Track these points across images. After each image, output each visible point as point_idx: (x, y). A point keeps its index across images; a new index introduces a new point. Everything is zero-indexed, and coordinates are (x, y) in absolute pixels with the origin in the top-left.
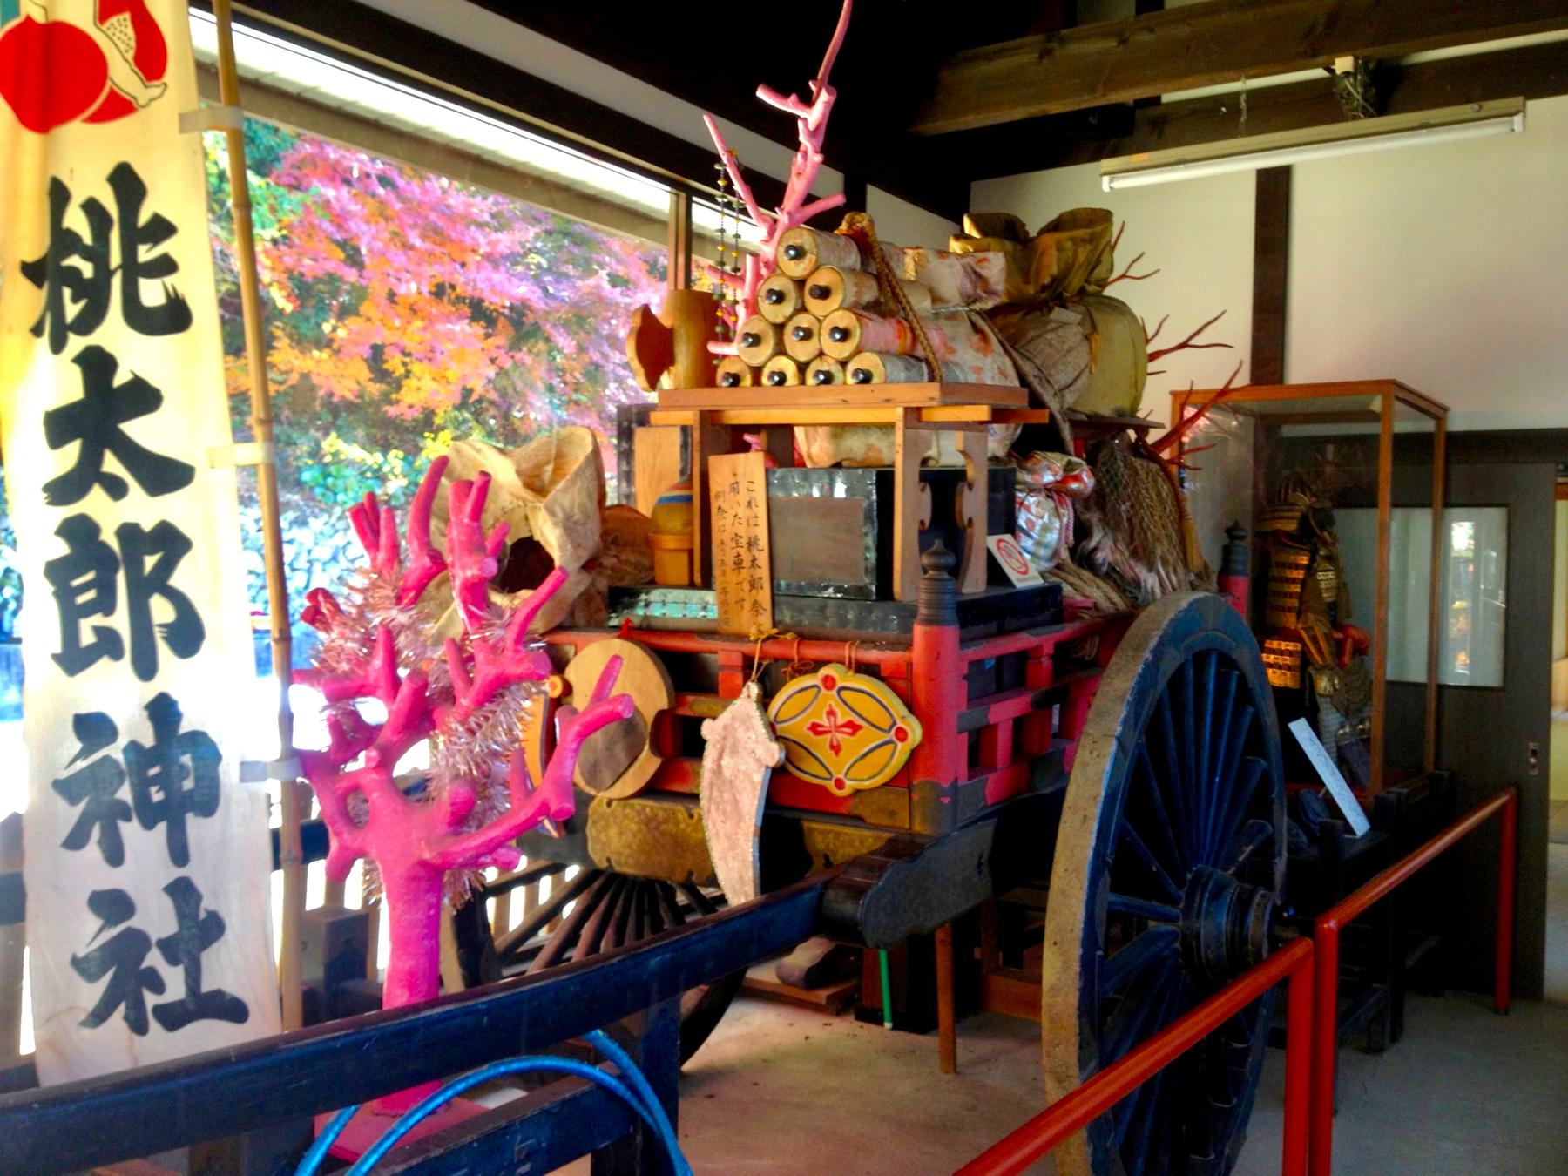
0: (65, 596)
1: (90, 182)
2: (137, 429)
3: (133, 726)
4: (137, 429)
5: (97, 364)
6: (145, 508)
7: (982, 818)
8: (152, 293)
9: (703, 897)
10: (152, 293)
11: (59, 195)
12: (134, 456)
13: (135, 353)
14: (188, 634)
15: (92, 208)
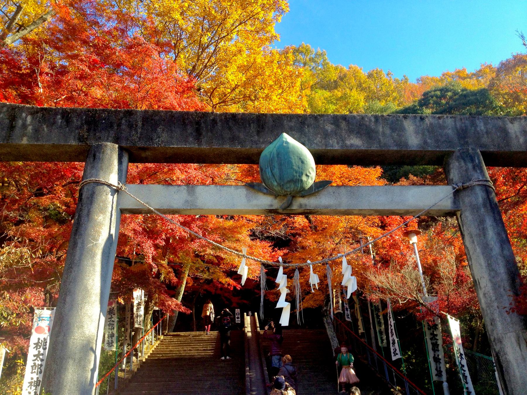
0: (32, 368)
5: (39, 352)
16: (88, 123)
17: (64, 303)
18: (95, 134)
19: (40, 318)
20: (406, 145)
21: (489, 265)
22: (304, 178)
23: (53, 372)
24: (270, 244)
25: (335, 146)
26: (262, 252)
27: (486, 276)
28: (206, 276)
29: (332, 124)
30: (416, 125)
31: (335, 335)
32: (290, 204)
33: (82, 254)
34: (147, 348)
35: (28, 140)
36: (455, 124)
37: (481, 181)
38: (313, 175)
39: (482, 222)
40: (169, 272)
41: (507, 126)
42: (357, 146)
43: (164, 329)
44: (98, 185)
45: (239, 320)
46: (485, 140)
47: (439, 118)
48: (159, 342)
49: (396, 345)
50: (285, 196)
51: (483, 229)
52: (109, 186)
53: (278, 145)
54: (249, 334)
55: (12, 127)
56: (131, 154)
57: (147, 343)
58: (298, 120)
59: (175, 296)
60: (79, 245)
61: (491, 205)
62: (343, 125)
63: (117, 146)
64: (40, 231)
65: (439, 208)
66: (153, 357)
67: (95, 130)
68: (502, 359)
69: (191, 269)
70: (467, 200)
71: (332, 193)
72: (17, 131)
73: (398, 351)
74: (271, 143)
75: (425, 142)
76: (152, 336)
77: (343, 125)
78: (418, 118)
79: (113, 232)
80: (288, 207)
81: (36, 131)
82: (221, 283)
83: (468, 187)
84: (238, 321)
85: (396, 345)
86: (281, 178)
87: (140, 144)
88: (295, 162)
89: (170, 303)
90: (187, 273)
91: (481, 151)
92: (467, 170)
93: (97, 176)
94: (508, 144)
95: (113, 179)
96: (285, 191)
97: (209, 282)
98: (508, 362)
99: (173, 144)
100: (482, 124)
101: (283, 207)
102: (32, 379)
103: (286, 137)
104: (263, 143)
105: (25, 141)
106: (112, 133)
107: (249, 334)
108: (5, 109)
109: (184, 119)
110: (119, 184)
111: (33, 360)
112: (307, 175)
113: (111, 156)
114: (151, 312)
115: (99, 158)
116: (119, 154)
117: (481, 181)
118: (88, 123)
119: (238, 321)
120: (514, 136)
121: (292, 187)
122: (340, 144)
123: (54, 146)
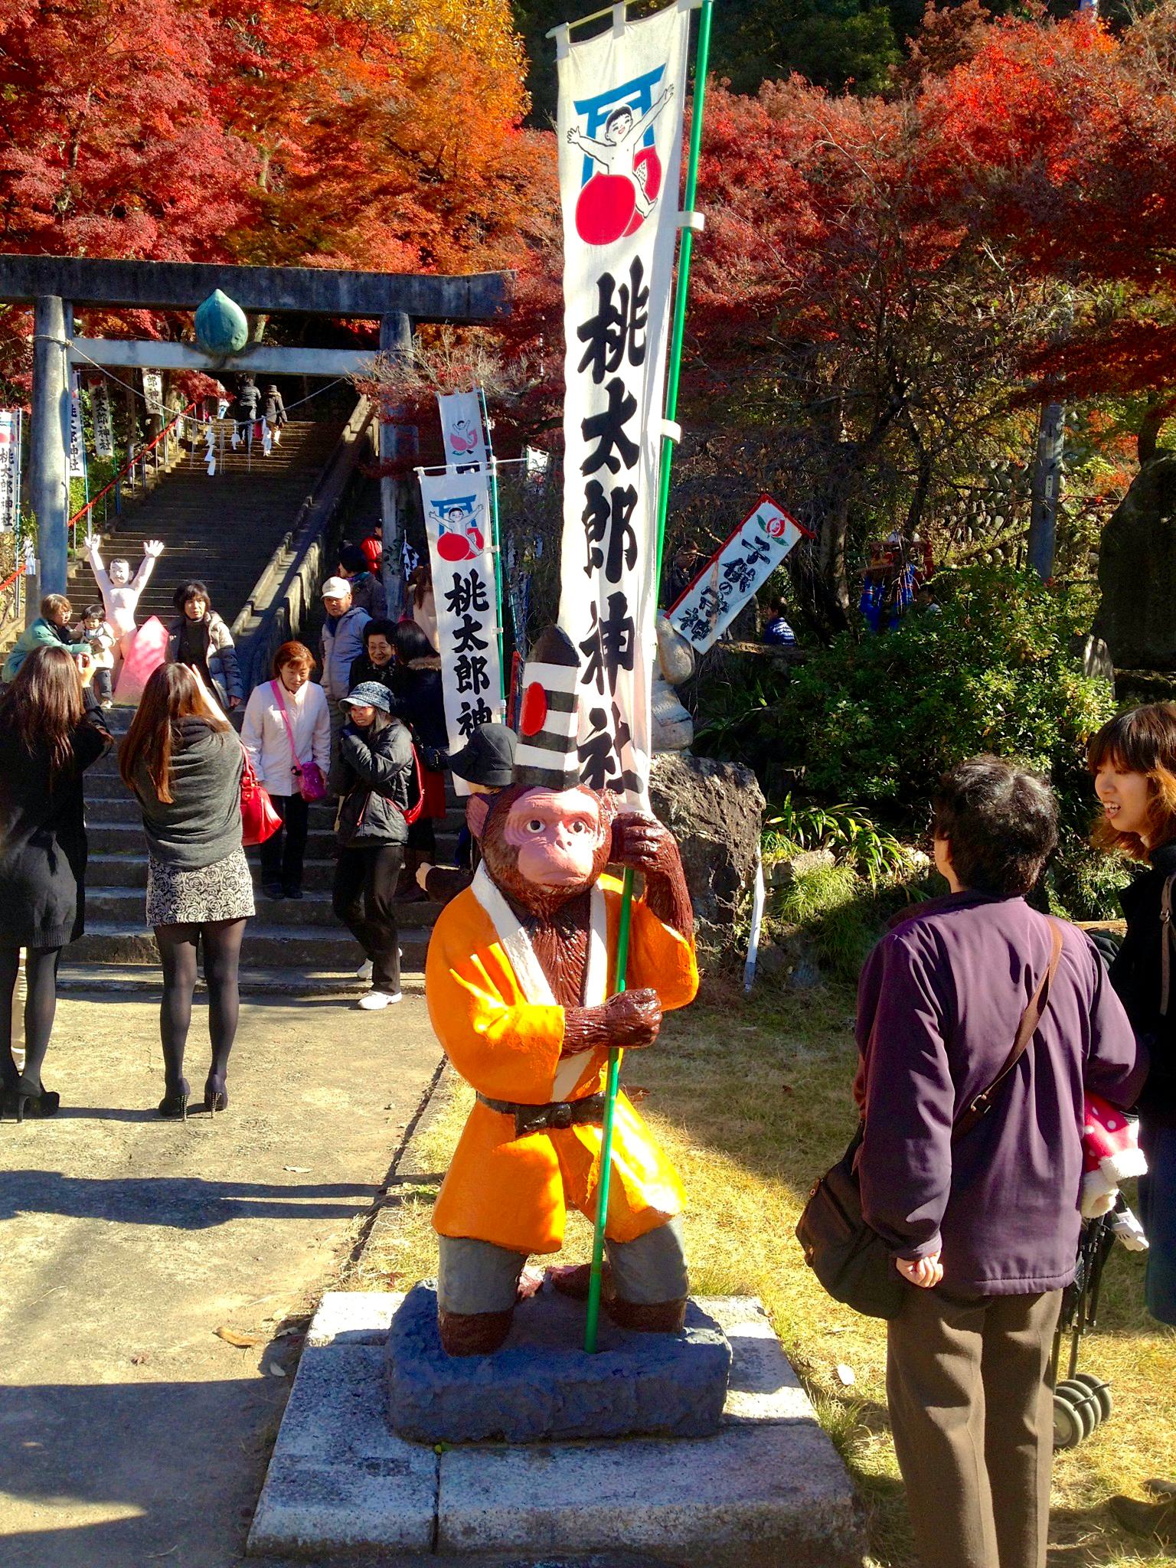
0: (459, 675)
1: (465, 575)
2: (477, 634)
3: (475, 706)
4: (477, 634)
5: (467, 618)
6: (478, 653)
7: (851, 1257)
8: (480, 601)
10: (480, 601)
11: (457, 577)
12: (475, 640)
14: (486, 683)
15: (466, 581)
22: (234, 341)
46: (416, 303)
56: (75, 307)
62: (278, 280)
75: (357, 304)
77: (278, 280)
88: (226, 325)
95: (60, 334)
102: (465, 706)
103: (220, 296)
106: (55, 285)
111: (457, 650)
120: (446, 300)
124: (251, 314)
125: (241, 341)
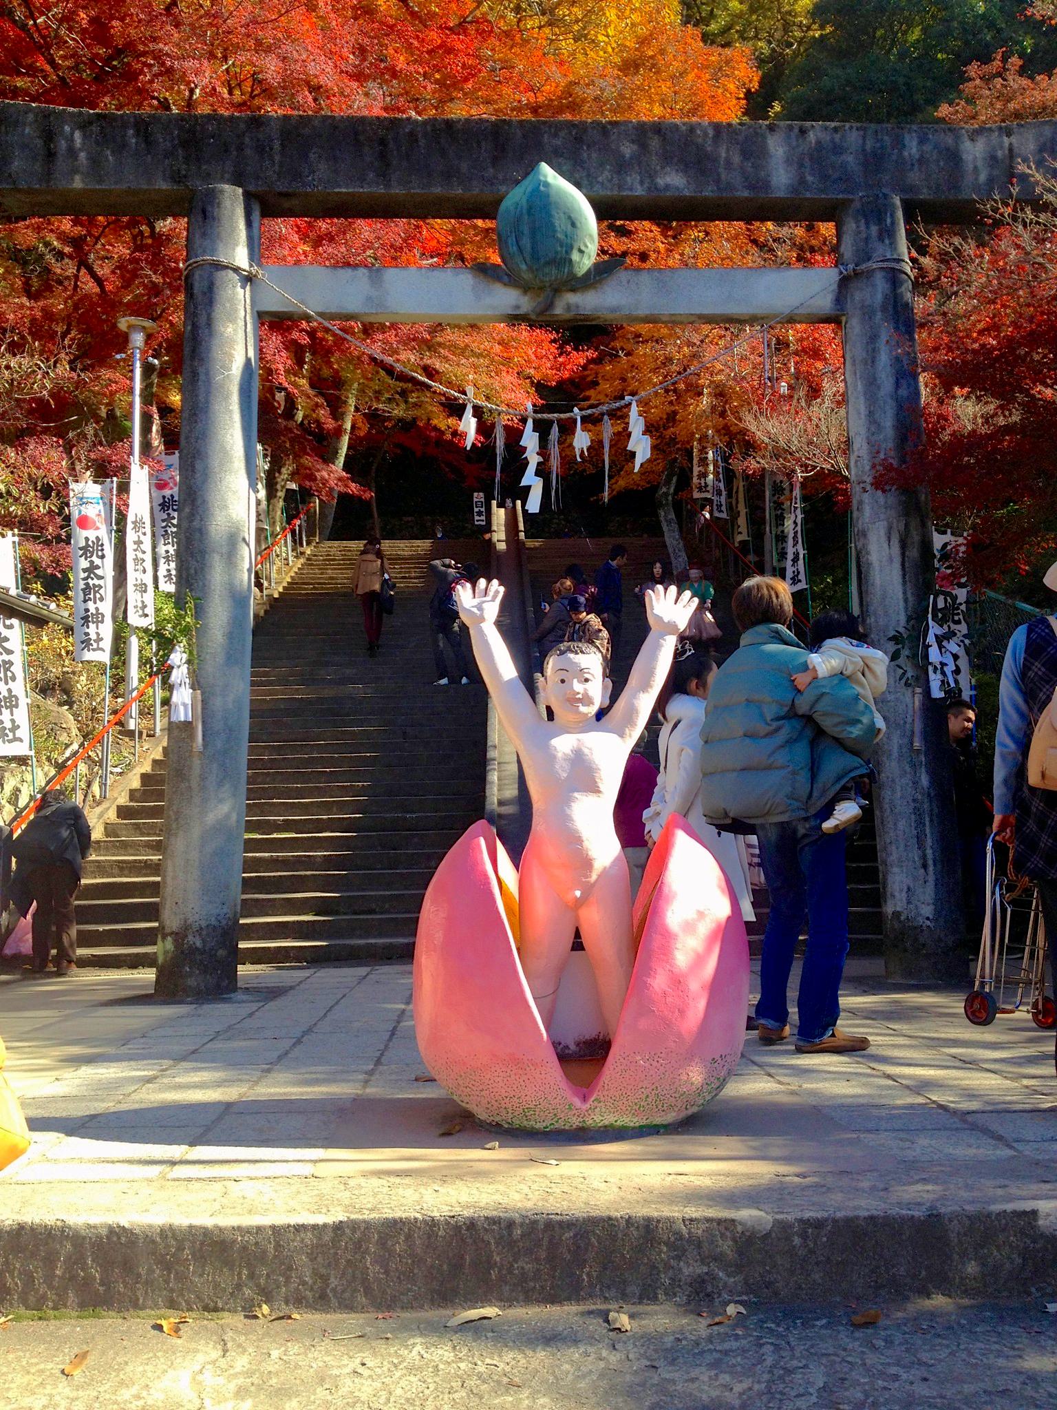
5: (91, 562)
6: (96, 582)
9: (597, 266)
13: (97, 561)
14: (14, 679)
16: (185, 144)
17: (193, 471)
18: (200, 168)
19: (83, 501)
20: (766, 185)
21: (871, 414)
22: (575, 256)
23: (192, 571)
24: (554, 336)
25: (636, 188)
26: (533, 357)
27: (863, 431)
28: (398, 412)
29: (633, 142)
30: (789, 145)
31: (681, 545)
32: (551, 305)
33: (208, 393)
34: (279, 571)
35: (83, 182)
36: (864, 143)
37: (888, 260)
38: (592, 248)
39: (873, 338)
40: (317, 405)
41: (962, 147)
42: (677, 189)
43: (311, 534)
44: (217, 270)
45: (483, 518)
46: (914, 177)
47: (836, 130)
48: (302, 560)
49: (801, 562)
50: (541, 289)
51: (874, 350)
52: (236, 270)
53: (529, 190)
54: (502, 546)
55: (51, 155)
56: (264, 205)
57: (277, 561)
58: (570, 133)
59: (328, 457)
60: (202, 377)
61: (895, 307)
62: (655, 143)
63: (240, 190)
64: (22, 306)
65: (809, 311)
66: (294, 589)
67: (198, 159)
68: (863, 560)
69: (362, 391)
70: (858, 296)
71: (625, 283)
72: (61, 164)
73: (802, 576)
74: (518, 182)
76: (286, 546)
77: (655, 143)
78: (796, 130)
79: (251, 354)
80: (547, 310)
81: (95, 161)
82: (436, 428)
83: (863, 272)
84: (479, 520)
85: (801, 562)
86: (535, 255)
87: (281, 187)
88: (560, 223)
89: (325, 474)
90: (352, 402)
91: (901, 200)
92: (867, 239)
93: (213, 251)
94: (955, 185)
95: (241, 257)
96: (542, 281)
97: (407, 425)
98: (869, 564)
99: (340, 186)
100: (915, 143)
101: (538, 310)
103: (548, 173)
104: (504, 181)
105: (78, 183)
107: (502, 546)
108: (31, 117)
109: (356, 134)
110: (251, 266)
112: (581, 251)
113: (233, 211)
114: (281, 494)
115: (214, 219)
116: (245, 208)
117: (888, 260)
118: (185, 144)
119: (479, 520)
121: (553, 273)
122: (646, 185)
123: (129, 192)
124: (604, 211)
125: (586, 257)
